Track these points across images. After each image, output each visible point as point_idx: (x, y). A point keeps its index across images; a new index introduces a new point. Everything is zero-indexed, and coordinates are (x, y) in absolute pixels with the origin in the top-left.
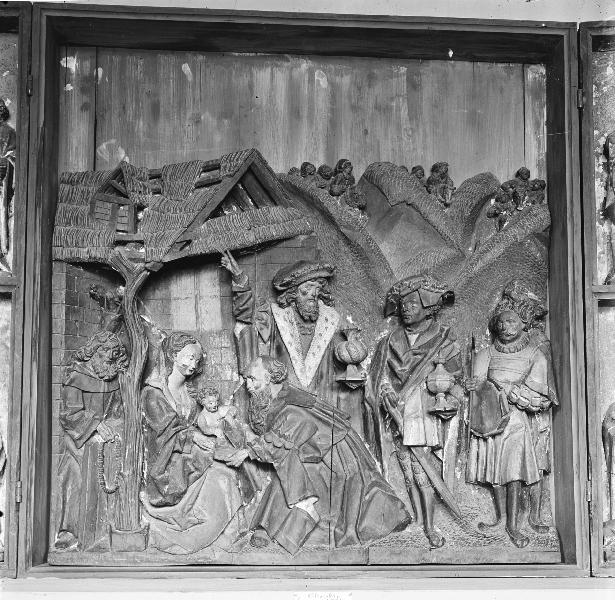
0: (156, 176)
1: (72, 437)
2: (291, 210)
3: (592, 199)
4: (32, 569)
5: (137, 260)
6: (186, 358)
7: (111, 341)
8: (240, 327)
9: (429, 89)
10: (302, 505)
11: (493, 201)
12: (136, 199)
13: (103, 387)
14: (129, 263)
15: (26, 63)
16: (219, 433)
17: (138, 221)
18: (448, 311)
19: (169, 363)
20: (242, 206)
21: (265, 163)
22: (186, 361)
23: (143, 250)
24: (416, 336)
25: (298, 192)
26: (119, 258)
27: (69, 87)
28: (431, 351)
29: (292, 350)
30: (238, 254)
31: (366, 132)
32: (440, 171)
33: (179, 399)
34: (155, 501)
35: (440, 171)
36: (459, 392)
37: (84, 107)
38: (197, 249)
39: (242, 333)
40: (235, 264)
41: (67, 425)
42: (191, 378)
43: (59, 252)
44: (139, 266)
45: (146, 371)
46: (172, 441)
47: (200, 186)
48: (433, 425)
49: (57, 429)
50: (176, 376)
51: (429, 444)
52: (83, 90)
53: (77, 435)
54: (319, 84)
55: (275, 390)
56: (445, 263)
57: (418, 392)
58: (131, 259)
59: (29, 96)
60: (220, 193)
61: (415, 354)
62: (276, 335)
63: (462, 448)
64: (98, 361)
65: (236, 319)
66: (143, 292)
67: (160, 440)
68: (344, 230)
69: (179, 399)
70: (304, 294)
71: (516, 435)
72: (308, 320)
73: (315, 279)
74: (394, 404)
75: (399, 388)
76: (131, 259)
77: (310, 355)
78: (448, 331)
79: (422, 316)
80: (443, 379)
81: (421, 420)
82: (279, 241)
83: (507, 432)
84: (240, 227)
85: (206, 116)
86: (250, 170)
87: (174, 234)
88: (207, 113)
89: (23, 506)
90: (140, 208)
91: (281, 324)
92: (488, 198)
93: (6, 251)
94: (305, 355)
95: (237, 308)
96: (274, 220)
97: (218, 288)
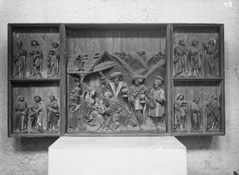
1: (71, 109)
2: (113, 62)
3: (173, 58)
8: (103, 86)
9: (6, 96)
12: (83, 61)
13: (77, 99)
19: (90, 94)
21: (108, 53)
25: (114, 58)
29: (114, 90)
34: (87, 121)
35: (144, 53)
36: (146, 98)
39: (104, 87)
41: (70, 106)
44: (83, 75)
45: (85, 95)
47: (95, 58)
51: (140, 109)
53: (72, 108)
56: (145, 71)
58: (82, 73)
59: (62, 42)
63: (147, 110)
68: (124, 66)
73: (118, 77)
75: (135, 98)
76: (82, 73)
77: (117, 91)
80: (143, 96)
84: (103, 66)
86: (105, 55)
87: (90, 69)
89: (63, 123)
90: (84, 63)
91: (111, 85)
93: (100, 57)
94: (116, 91)
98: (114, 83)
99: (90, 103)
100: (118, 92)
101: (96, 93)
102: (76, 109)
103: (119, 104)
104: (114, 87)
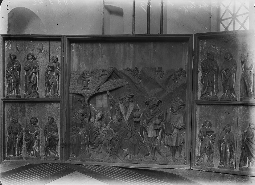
0: (92, 72)
4: (2, 37)
5: (89, 92)
6: (99, 115)
7: (81, 110)
8: (111, 107)
10: (125, 150)
11: (173, 76)
14: (86, 94)
15: (62, 47)
16: (106, 132)
17: (88, 84)
18: (160, 104)
19: (95, 117)
20: (113, 79)
22: (99, 116)
23: (89, 90)
24: (152, 111)
26: (84, 93)
27: (73, 50)
28: (155, 114)
29: (123, 113)
30: (110, 91)
31: (142, 59)
32: (161, 69)
33: (97, 124)
35: (161, 69)
37: (77, 55)
38: (100, 91)
39: (112, 108)
40: (110, 94)
41: (73, 130)
42: (101, 119)
43: (71, 91)
44: (88, 94)
46: (96, 135)
48: (155, 132)
49: (71, 131)
50: (96, 119)
52: (76, 51)
53: (75, 132)
54: (131, 47)
55: (119, 123)
57: (152, 124)
60: (107, 76)
61: (151, 115)
62: (119, 109)
64: (79, 116)
65: (111, 105)
66: (89, 101)
67: (94, 134)
69: (97, 124)
70: (126, 101)
71: (175, 134)
72: (127, 107)
74: (146, 127)
78: (160, 109)
79: (153, 106)
80: (157, 121)
81: (152, 131)
82: (120, 87)
83: (173, 134)
84: (110, 84)
85: (104, 56)
87: (96, 88)
88: (105, 55)
90: (89, 81)
92: (172, 75)
95: (111, 103)
96: (119, 82)
97: (107, 97)
98: (124, 104)
99: (95, 128)
100: (128, 116)
101: (102, 116)
102: (80, 133)
103: (129, 130)
104: (124, 110)
